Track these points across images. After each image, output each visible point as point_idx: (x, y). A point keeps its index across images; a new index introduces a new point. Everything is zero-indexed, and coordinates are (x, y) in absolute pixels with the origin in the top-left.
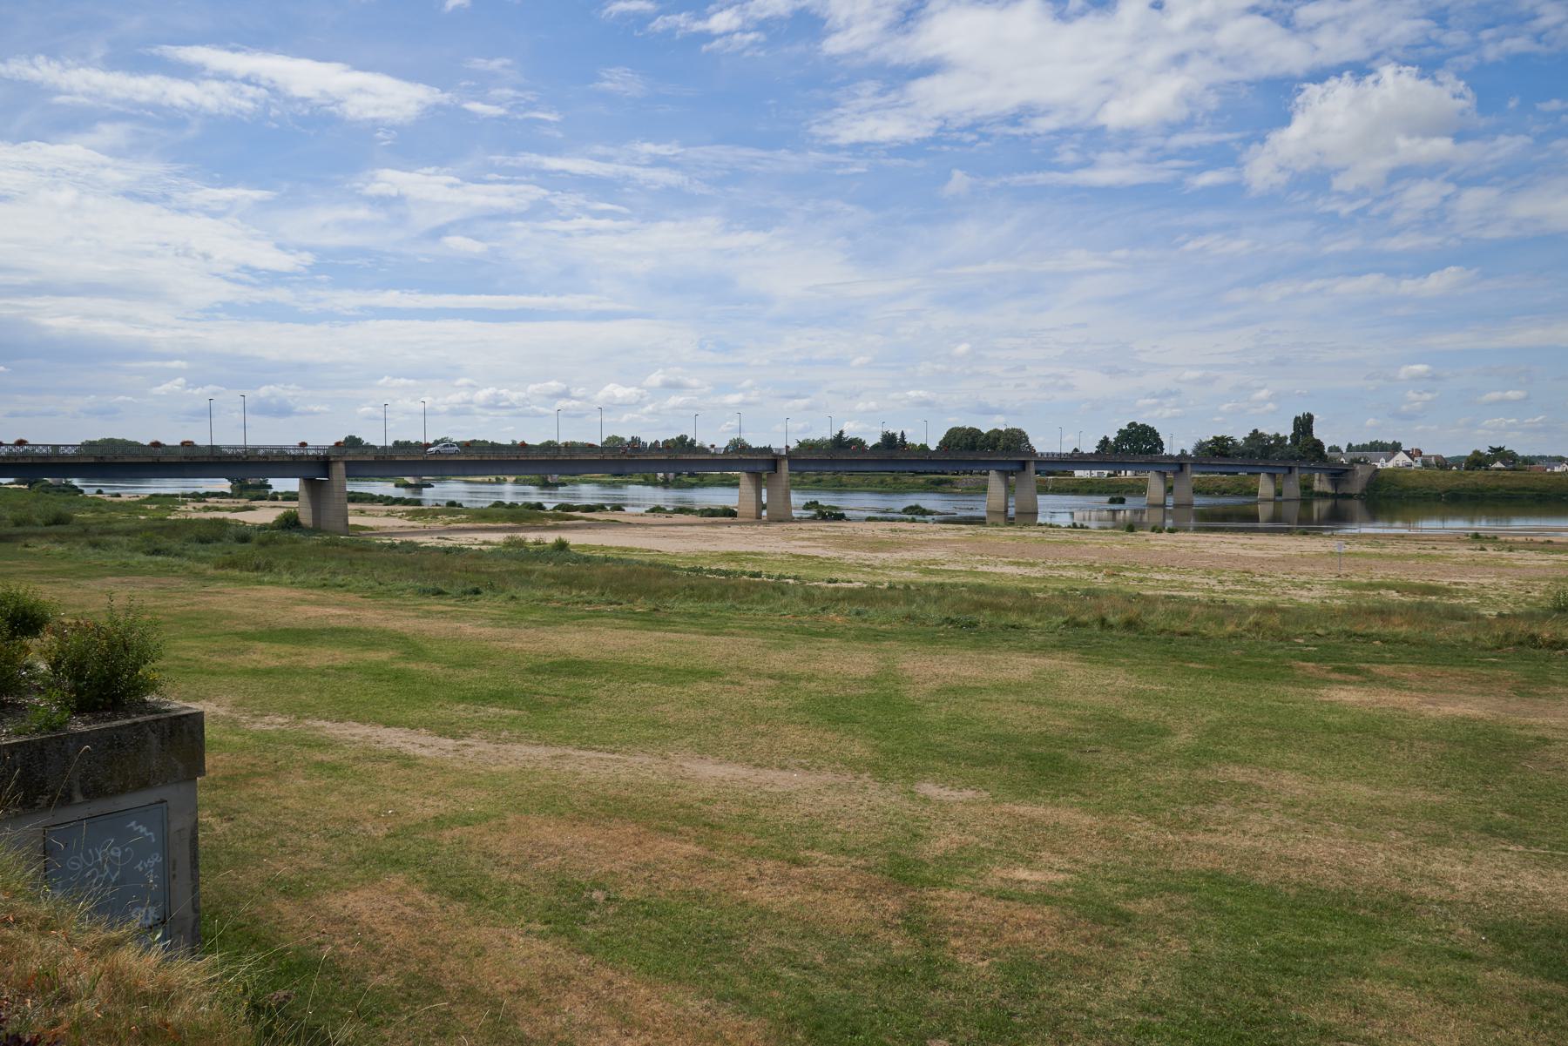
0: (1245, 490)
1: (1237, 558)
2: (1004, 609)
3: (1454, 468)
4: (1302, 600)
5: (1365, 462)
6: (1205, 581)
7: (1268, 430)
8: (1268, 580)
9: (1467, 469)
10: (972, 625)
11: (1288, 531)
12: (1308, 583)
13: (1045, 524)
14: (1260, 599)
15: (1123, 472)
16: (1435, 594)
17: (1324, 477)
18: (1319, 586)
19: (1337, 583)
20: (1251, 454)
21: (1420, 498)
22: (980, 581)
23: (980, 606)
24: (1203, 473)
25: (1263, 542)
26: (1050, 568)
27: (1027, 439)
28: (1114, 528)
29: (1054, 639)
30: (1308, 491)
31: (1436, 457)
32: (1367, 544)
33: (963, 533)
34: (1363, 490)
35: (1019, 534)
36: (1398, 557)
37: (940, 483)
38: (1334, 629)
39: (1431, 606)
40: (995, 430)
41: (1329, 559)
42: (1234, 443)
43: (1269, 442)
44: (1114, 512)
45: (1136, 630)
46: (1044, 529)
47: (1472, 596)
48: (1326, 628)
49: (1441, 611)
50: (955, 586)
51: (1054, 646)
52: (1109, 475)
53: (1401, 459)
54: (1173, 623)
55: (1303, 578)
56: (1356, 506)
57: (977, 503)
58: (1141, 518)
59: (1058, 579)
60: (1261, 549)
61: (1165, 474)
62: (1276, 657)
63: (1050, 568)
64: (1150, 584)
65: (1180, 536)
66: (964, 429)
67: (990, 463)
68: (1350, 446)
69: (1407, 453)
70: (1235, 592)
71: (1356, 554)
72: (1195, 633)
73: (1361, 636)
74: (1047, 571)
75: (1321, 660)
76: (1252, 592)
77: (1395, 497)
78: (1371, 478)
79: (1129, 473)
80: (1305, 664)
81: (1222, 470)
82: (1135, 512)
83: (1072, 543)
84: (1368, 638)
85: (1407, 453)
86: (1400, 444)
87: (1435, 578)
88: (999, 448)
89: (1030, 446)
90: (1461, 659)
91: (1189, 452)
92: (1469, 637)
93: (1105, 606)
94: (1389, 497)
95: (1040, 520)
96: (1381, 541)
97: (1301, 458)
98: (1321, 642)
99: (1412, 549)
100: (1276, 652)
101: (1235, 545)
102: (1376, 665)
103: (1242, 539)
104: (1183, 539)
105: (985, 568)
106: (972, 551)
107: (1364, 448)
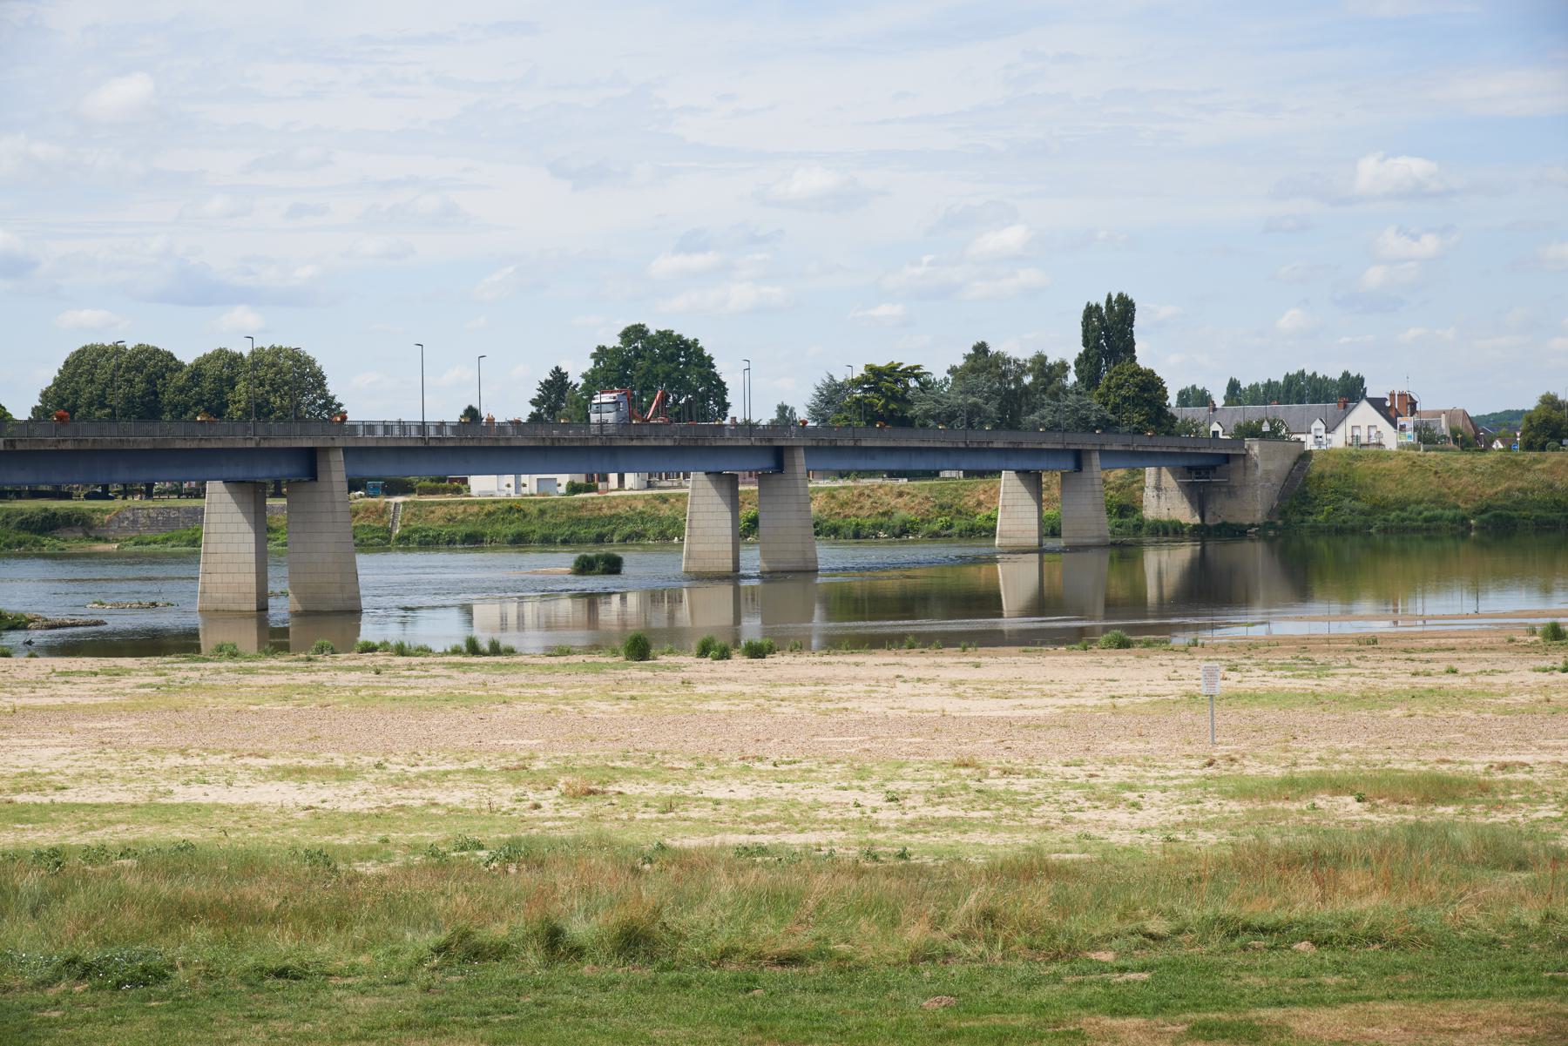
0: (960, 524)
1: (938, 725)
2: (255, 920)
3: (1498, 445)
4: (1114, 838)
5: (1274, 434)
6: (851, 796)
7: (1016, 346)
8: (1021, 784)
9: (1529, 446)
10: (152, 976)
11: (1077, 639)
12: (1131, 788)
13: (385, 646)
14: (1003, 843)
15: (613, 477)
16: (1453, 799)
17: (1168, 479)
18: (1157, 795)
19: (1204, 784)
20: (973, 415)
21: (1416, 530)
22: (180, 833)
23: (182, 913)
24: (842, 475)
25: (1011, 673)
26: (399, 782)
27: (319, 380)
28: (594, 648)
29: (408, 1001)
30: (1132, 520)
31: (1451, 415)
32: (1282, 667)
33: (125, 683)
34: (1271, 512)
35: (303, 679)
36: (1363, 700)
37: (49, 524)
38: (1191, 914)
39: (1441, 833)
40: (221, 353)
41: (1186, 716)
42: (924, 386)
43: (1018, 380)
44: (592, 600)
45: (652, 958)
46: (380, 659)
47: (1542, 800)
48: (1173, 914)
49: (1468, 845)
50: (98, 854)
51: (408, 1025)
52: (574, 489)
53: (1363, 418)
54: (755, 928)
55: (1117, 774)
56: (1255, 556)
57: (167, 586)
58: (672, 617)
59: (422, 817)
60: (1006, 695)
61: (733, 481)
62: (1041, 1008)
63: (399, 782)
64: (695, 814)
65: (782, 664)
66: (118, 351)
67: (205, 461)
68: (1233, 386)
69: (1378, 404)
70: (934, 823)
71: (1254, 697)
72: (820, 955)
73: (1263, 930)
74: (392, 794)
75: (1160, 1008)
76: (981, 824)
77: (1353, 531)
78: (1290, 478)
79: (630, 479)
80: (1117, 1022)
81: (895, 464)
82: (654, 597)
83: (467, 701)
84: (1278, 933)
85: (1378, 404)
86: (1360, 380)
87: (1455, 755)
88: (235, 411)
89: (329, 401)
90: (1512, 976)
91: (802, 414)
92: (1530, 916)
93: (563, 890)
94: (1340, 531)
95: (369, 631)
96: (1319, 658)
97: (1107, 426)
98: (1158, 955)
99: (1396, 676)
100: (1041, 994)
101: (935, 687)
102: (1301, 1011)
103: (951, 666)
104: (789, 672)
105: (196, 794)
106: (151, 742)
107: (1270, 393)
